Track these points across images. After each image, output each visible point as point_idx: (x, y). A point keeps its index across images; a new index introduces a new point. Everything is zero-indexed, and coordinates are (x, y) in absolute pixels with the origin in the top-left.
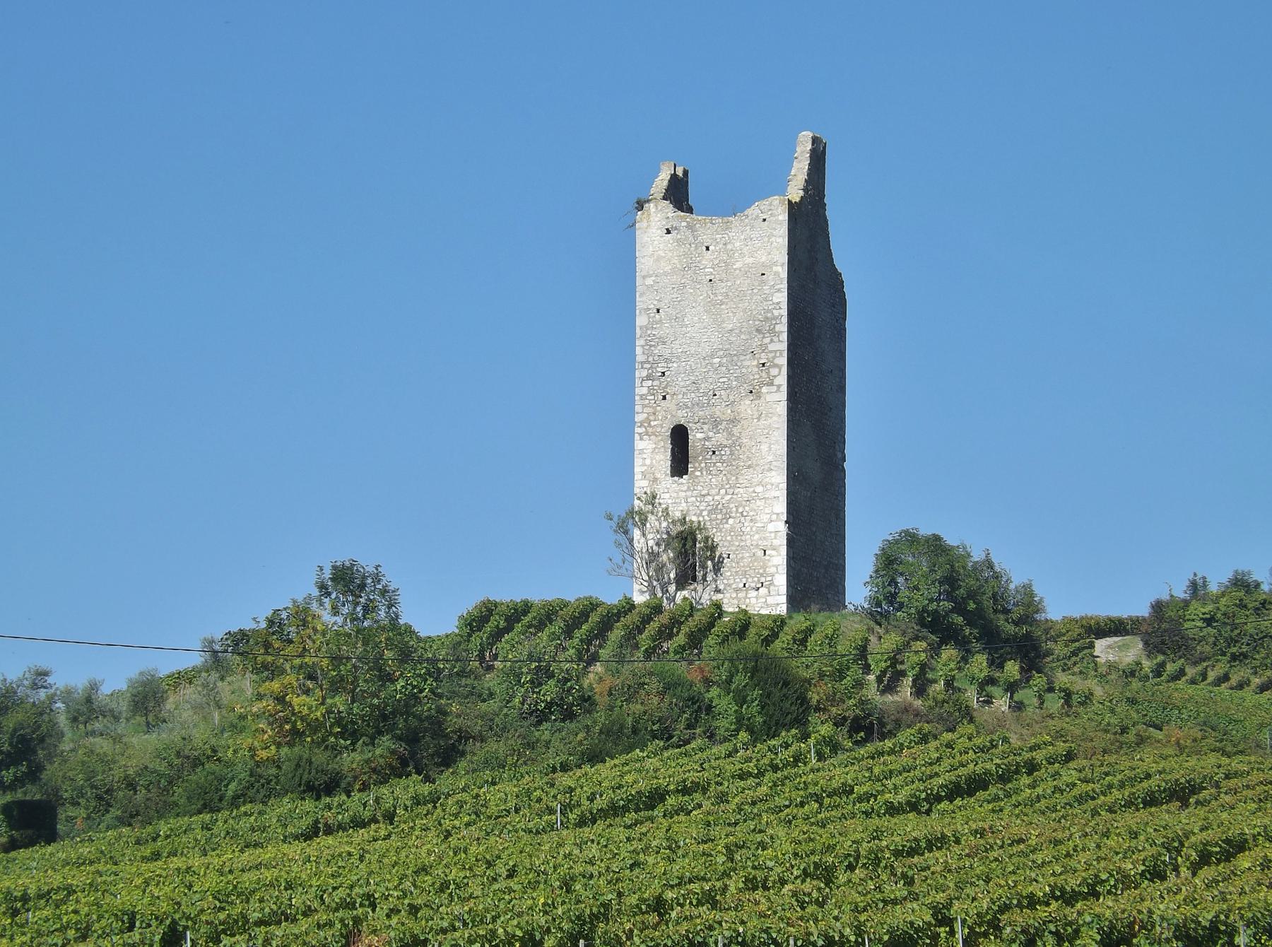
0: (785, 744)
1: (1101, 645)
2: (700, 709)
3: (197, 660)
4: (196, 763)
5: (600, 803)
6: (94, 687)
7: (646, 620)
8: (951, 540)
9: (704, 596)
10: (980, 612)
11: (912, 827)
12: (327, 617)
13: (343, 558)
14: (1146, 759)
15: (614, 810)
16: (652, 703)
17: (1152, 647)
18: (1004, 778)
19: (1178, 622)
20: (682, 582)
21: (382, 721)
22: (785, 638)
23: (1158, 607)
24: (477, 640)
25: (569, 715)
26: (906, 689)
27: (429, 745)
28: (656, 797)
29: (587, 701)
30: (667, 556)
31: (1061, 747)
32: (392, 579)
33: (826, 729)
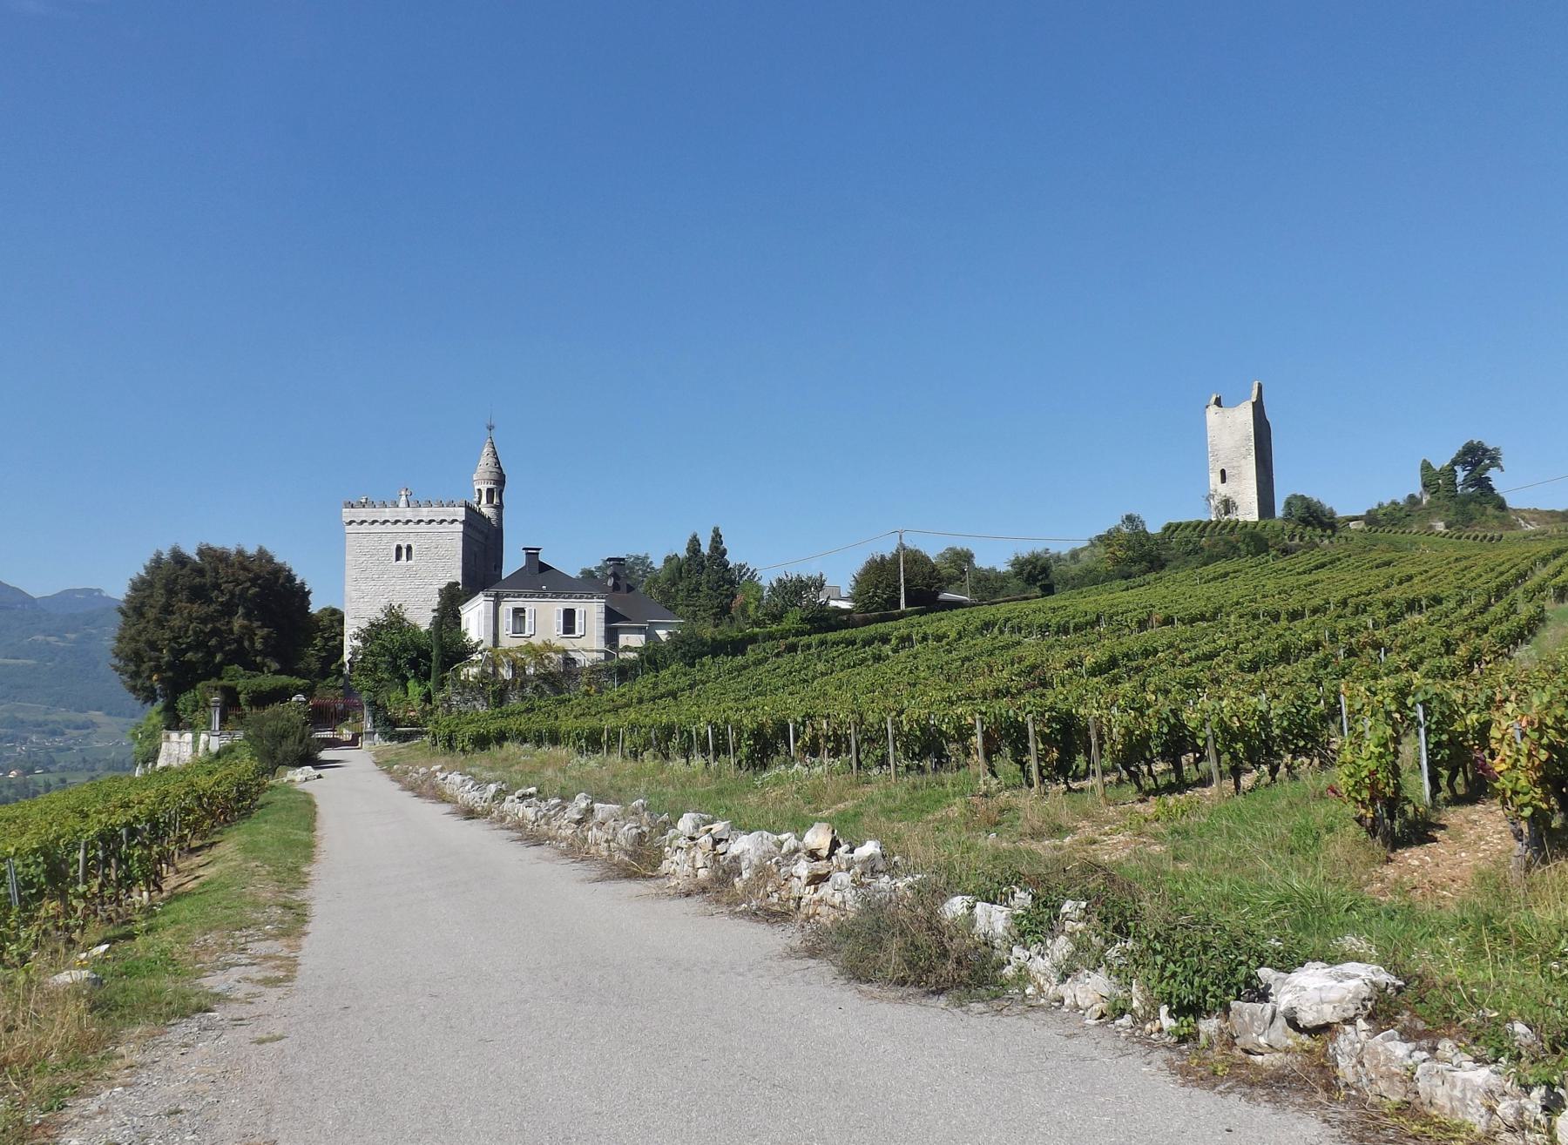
0: (1262, 558)
1: (1351, 524)
2: (1235, 549)
3: (1087, 544)
4: (1091, 572)
5: (1210, 577)
6: (1059, 553)
7: (1217, 525)
8: (1307, 496)
9: (1233, 517)
10: (1317, 516)
11: (1307, 578)
12: (1125, 530)
13: (1128, 513)
14: (1373, 555)
15: (1215, 579)
16: (1221, 548)
17: (1367, 524)
18: (1331, 563)
19: (1376, 515)
20: (1226, 514)
21: (1142, 558)
22: (1258, 528)
23: (1369, 512)
24: (1168, 533)
25: (1197, 553)
26: (1297, 540)
27: (1156, 564)
28: (1227, 574)
29: (1202, 548)
30: (1221, 507)
31: (1347, 553)
32: (1143, 518)
33: (1274, 553)
